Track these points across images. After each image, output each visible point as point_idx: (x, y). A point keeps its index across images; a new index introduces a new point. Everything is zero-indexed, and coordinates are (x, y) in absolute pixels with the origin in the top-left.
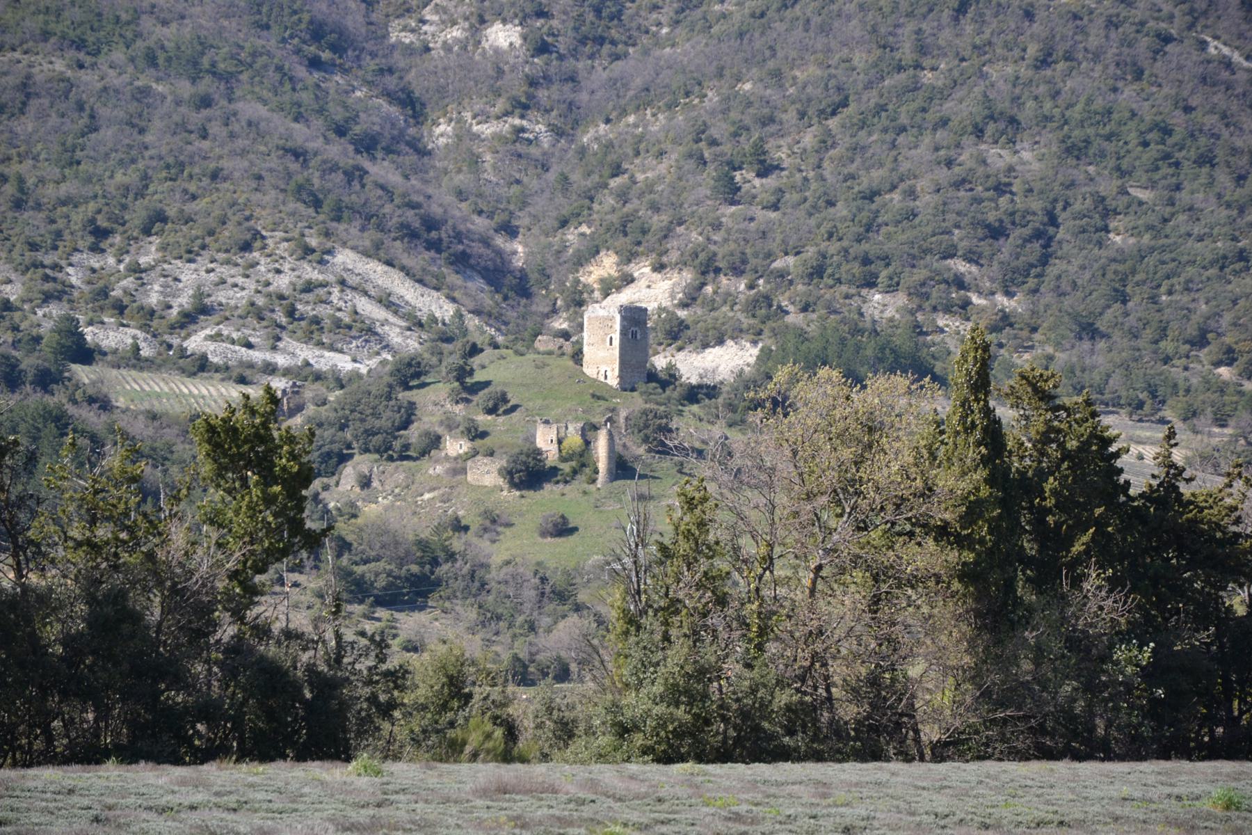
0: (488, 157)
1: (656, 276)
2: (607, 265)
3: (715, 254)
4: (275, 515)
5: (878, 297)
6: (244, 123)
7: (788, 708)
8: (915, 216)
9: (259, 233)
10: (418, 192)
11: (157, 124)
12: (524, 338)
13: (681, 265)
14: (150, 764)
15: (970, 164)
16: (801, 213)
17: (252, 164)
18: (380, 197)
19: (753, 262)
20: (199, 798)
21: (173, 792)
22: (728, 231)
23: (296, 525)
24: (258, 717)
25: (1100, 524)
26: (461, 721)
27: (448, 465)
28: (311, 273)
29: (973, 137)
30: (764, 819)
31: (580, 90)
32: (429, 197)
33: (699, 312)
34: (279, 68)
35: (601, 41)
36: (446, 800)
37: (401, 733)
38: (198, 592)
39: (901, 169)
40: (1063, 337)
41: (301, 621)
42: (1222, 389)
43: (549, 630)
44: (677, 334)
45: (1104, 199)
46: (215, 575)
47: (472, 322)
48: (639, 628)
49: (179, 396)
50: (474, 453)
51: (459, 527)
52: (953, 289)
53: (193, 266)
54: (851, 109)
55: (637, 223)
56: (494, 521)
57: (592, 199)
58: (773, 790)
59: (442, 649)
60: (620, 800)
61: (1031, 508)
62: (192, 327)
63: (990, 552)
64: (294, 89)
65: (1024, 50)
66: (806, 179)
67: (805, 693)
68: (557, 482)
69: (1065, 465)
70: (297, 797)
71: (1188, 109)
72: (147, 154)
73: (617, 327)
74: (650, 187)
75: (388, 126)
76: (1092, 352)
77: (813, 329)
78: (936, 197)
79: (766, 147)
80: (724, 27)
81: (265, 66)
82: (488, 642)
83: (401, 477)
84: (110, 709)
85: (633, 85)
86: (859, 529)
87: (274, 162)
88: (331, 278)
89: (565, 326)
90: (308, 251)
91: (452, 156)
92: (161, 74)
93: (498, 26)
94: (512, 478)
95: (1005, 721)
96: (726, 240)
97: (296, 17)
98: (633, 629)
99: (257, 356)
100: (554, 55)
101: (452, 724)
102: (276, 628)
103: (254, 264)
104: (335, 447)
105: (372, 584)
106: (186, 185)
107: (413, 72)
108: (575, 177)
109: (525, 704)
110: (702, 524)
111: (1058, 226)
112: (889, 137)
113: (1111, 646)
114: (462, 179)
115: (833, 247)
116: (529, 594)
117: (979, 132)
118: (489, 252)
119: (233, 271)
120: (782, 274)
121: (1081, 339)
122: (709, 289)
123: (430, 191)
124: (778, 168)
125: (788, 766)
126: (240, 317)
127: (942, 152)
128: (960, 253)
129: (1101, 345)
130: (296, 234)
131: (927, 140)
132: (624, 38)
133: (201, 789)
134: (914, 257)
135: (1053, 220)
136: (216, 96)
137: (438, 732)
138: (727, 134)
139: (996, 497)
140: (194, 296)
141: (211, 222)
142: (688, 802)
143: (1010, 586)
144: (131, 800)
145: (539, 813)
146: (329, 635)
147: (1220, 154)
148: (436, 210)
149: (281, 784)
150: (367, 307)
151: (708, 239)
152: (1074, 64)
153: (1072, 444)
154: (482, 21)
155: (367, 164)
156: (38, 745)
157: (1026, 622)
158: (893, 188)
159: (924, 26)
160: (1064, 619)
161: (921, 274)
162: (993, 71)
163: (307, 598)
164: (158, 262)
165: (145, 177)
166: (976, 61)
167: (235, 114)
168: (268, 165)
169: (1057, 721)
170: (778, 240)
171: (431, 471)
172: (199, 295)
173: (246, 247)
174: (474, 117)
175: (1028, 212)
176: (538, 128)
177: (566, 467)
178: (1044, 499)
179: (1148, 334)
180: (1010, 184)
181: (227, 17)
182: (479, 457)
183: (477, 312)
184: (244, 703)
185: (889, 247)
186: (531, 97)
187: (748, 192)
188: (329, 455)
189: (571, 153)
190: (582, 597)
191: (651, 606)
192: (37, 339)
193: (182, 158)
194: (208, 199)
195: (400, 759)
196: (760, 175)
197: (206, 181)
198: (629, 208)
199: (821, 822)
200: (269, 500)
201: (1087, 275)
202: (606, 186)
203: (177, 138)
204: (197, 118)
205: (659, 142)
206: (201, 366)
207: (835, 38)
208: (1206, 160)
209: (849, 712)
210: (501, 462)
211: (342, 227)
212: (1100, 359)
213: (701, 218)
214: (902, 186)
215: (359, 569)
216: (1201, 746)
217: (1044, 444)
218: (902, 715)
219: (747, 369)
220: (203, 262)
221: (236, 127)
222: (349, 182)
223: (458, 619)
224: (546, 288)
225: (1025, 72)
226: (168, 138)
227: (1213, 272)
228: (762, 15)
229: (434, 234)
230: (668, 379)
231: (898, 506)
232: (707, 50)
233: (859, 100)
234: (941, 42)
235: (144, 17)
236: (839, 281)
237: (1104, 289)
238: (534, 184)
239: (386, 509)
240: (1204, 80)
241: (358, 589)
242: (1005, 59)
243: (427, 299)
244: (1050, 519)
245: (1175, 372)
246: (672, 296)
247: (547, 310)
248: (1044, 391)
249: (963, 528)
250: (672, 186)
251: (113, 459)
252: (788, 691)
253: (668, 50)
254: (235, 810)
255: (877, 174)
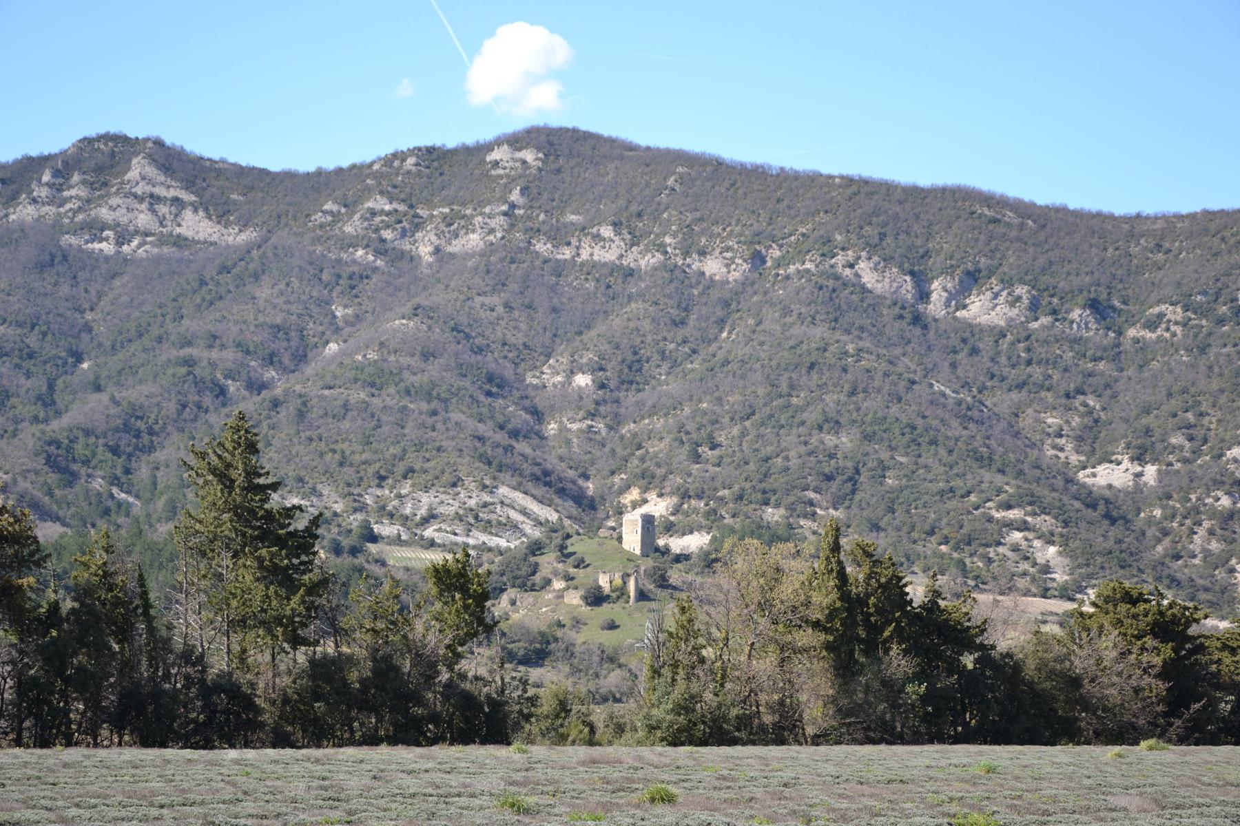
0: (575, 440)
2: (634, 494)
7: (737, 717)
11: (411, 424)
12: (593, 530)
13: (672, 494)
15: (816, 444)
16: (731, 468)
19: (708, 492)
20: (430, 765)
23: (481, 621)
25: (898, 621)
34: (471, 396)
35: (631, 382)
37: (535, 730)
41: (482, 671)
42: (942, 556)
44: (669, 528)
47: (567, 522)
48: (659, 675)
50: (568, 588)
51: (561, 625)
54: (756, 417)
58: (738, 762)
59: (553, 687)
61: (862, 613)
71: (924, 417)
73: (640, 524)
74: (656, 455)
77: (737, 527)
82: (575, 683)
83: (531, 600)
84: (383, 717)
87: (468, 443)
88: (496, 500)
90: (485, 487)
93: (580, 375)
95: (850, 724)
99: (459, 539)
101: (562, 725)
102: (470, 675)
103: (458, 494)
104: (498, 585)
108: (618, 450)
109: (599, 714)
110: (690, 621)
112: (776, 430)
113: (904, 685)
114: (562, 451)
115: (748, 485)
116: (596, 659)
117: (820, 428)
120: (722, 499)
122: (685, 506)
125: (739, 748)
129: (882, 534)
131: (794, 431)
135: (858, 472)
141: (437, 473)
143: (852, 652)
144: (393, 767)
146: (498, 679)
147: (941, 439)
148: (549, 467)
150: (514, 515)
153: (883, 580)
154: (572, 372)
155: (514, 444)
156: (346, 735)
157: (860, 673)
160: (880, 671)
161: (791, 499)
162: (827, 398)
164: (410, 493)
165: (404, 450)
166: (819, 393)
172: (431, 509)
173: (454, 485)
175: (845, 468)
177: (614, 595)
179: (905, 529)
183: (569, 517)
184: (453, 714)
185: (775, 485)
186: (596, 410)
190: (622, 660)
192: (350, 531)
196: (711, 449)
197: (434, 452)
200: (466, 607)
201: (875, 499)
206: (432, 544)
208: (933, 442)
209: (768, 719)
210: (582, 593)
215: (510, 646)
216: (950, 737)
220: (432, 492)
221: (449, 425)
225: (843, 398)
227: (937, 498)
230: (666, 551)
237: (883, 506)
238: (598, 454)
240: (932, 403)
244: (873, 619)
245: (919, 548)
250: (667, 454)
251: (386, 587)
255: (769, 449)
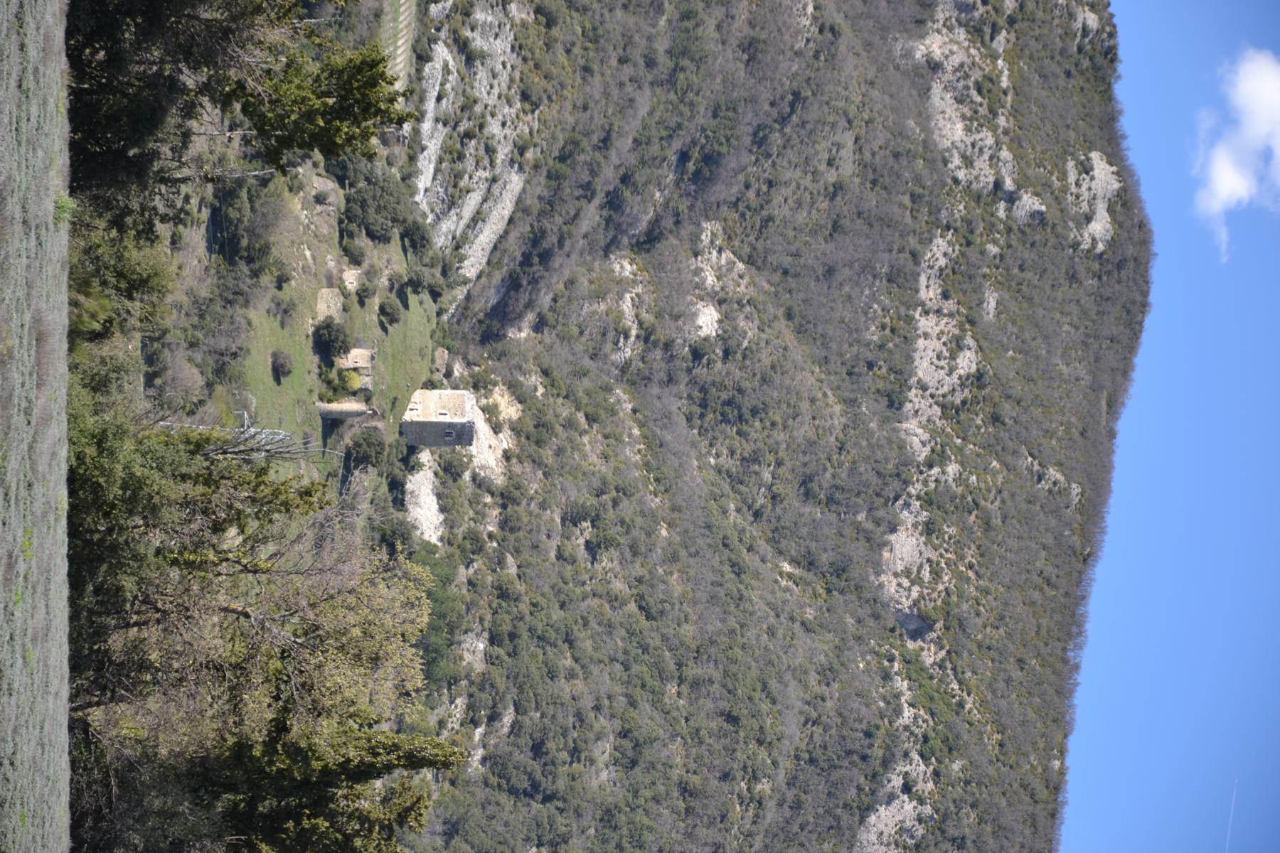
0: (603, 307)
1: (499, 453)
2: (509, 410)
3: (518, 504)
4: (295, 122)
5: (481, 646)
6: (632, 95)
7: (120, 589)
8: (552, 679)
9: (537, 107)
10: (573, 246)
11: (631, 20)
13: (510, 475)
14: (66, 8)
15: (597, 726)
16: (554, 579)
17: (597, 102)
18: (568, 213)
19: (512, 537)
20: (32, 52)
21: (38, 29)
22: (538, 516)
23: (286, 142)
24: (110, 107)
26: (107, 292)
27: (335, 271)
28: (502, 153)
29: (620, 728)
30: (10, 591)
31: (661, 387)
32: (568, 256)
33: (468, 491)
34: (679, 126)
35: (704, 405)
36: (29, 285)
37: (96, 237)
38: (225, 53)
39: (592, 667)
40: (446, 808)
41: (198, 145)
43: (190, 360)
44: (450, 471)
45: (566, 842)
46: (241, 68)
47: (460, 293)
48: (192, 453)
49: (395, 37)
50: (345, 294)
51: (281, 282)
52: (488, 712)
53: (509, 50)
54: (644, 623)
55: (545, 436)
56: (285, 312)
57: (566, 397)
58: (40, 589)
59: (174, 268)
60: (31, 448)
61: (301, 806)
62: (455, 49)
63: (262, 771)
64: (662, 139)
65: (695, 773)
66: (584, 583)
67: (133, 604)
68: (320, 367)
69: (339, 836)
70: (33, 145)
72: (606, 11)
73: (457, 420)
74: (577, 448)
75: (630, 220)
76: (433, 833)
77: (453, 590)
78: (568, 697)
79: (612, 549)
80: (715, 512)
81: (681, 114)
85: (665, 432)
86: (284, 651)
87: (599, 121)
88: (498, 170)
89: (456, 374)
90: (522, 150)
91: (604, 276)
92: (674, 24)
94: (324, 328)
95: (108, 785)
96: (530, 514)
97: (724, 141)
98: (192, 447)
99: (430, 105)
100: (691, 365)
101: (104, 283)
102: (193, 124)
103: (510, 103)
105: (231, 205)
106: (579, 44)
107: (675, 242)
108: (586, 383)
109: (126, 348)
110: (286, 505)
111: (542, 803)
114: (584, 282)
115: (524, 607)
116: (222, 343)
118: (521, 307)
119: (504, 86)
120: (501, 563)
121: (445, 823)
122: (488, 499)
123: (574, 256)
124: (594, 559)
125: (65, 592)
126: (464, 91)
127: (606, 702)
128: (519, 718)
129: (439, 842)
130: (536, 139)
131: (618, 689)
132: (706, 425)
133: (41, 54)
134: (516, 678)
135: (547, 799)
136: (655, 71)
137: (98, 271)
138: (623, 514)
139: (311, 776)
140: (482, 51)
141: (547, 66)
142: (28, 513)
143: (231, 787)
145: (16, 376)
146: (186, 172)
148: (557, 262)
149: (46, 129)
151: (532, 498)
152: (683, 816)
154: (721, 302)
155: (597, 201)
158: (576, 660)
159: (716, 686)
160: (199, 838)
161: (501, 683)
163: (219, 149)
164: (512, 20)
167: (640, 87)
168: (596, 116)
169: (106, 832)
170: (530, 559)
171: (329, 257)
172: (483, 56)
173: (525, 97)
174: (637, 295)
176: (628, 351)
177: (333, 375)
178: (309, 819)
180: (579, 761)
181: (724, 81)
182: (342, 298)
183: (468, 297)
185: (524, 655)
186: (655, 344)
187: (573, 533)
188: (344, 168)
189: (606, 378)
190: (219, 389)
191: (212, 463)
193: (602, 41)
194: (566, 63)
195: (73, 237)
197: (582, 62)
198: (559, 429)
199: (6, 646)
200: (310, 115)
201: (500, 829)
202: (578, 409)
203: (620, 38)
204: (637, 54)
205: (616, 456)
206: (422, 57)
207: (706, 608)
211: (543, 180)
212: (426, 840)
213: (550, 492)
214: (577, 668)
217: (359, 818)
218: (113, 692)
219: (418, 533)
220: (512, 59)
222: (581, 186)
223: (200, 280)
224: (490, 357)
225: (676, 774)
226: (619, 29)
228: (725, 545)
229: (536, 260)
230: (409, 462)
231: (303, 685)
232: (696, 497)
233: (652, 630)
234: (701, 701)
235: (724, 9)
236: (495, 613)
239: (297, 218)
241: (226, 193)
242: (687, 757)
243: (480, 253)
246: (482, 467)
247: (470, 357)
248: (406, 817)
249: (284, 745)
250: (578, 467)
252: (135, 588)
253: (696, 463)
254: (20, 86)
255: (588, 644)
